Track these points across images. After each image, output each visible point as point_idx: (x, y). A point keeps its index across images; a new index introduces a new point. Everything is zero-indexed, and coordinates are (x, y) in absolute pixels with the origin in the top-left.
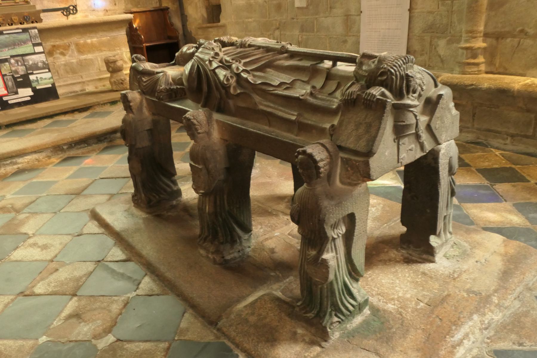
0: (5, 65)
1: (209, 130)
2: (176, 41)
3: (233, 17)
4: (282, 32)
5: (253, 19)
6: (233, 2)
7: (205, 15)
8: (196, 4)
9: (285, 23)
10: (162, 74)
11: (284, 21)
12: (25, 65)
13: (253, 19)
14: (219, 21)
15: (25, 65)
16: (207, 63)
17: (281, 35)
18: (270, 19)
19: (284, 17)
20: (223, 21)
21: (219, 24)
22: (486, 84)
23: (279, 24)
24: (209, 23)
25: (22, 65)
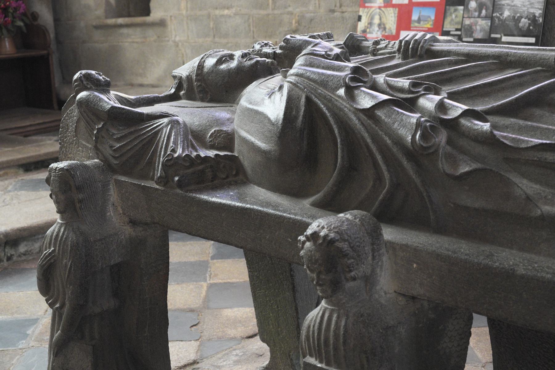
0: (456, 10)
1: (373, 271)
2: (45, 52)
5: (234, 10)
10: (166, 120)
11: (308, 15)
12: (492, 19)
13: (234, 10)
14: (147, 12)
15: (492, 19)
16: (342, 92)
18: (276, 12)
20: (156, 14)
21: (148, 19)
23: (299, 23)
24: (120, 15)
25: (486, 17)
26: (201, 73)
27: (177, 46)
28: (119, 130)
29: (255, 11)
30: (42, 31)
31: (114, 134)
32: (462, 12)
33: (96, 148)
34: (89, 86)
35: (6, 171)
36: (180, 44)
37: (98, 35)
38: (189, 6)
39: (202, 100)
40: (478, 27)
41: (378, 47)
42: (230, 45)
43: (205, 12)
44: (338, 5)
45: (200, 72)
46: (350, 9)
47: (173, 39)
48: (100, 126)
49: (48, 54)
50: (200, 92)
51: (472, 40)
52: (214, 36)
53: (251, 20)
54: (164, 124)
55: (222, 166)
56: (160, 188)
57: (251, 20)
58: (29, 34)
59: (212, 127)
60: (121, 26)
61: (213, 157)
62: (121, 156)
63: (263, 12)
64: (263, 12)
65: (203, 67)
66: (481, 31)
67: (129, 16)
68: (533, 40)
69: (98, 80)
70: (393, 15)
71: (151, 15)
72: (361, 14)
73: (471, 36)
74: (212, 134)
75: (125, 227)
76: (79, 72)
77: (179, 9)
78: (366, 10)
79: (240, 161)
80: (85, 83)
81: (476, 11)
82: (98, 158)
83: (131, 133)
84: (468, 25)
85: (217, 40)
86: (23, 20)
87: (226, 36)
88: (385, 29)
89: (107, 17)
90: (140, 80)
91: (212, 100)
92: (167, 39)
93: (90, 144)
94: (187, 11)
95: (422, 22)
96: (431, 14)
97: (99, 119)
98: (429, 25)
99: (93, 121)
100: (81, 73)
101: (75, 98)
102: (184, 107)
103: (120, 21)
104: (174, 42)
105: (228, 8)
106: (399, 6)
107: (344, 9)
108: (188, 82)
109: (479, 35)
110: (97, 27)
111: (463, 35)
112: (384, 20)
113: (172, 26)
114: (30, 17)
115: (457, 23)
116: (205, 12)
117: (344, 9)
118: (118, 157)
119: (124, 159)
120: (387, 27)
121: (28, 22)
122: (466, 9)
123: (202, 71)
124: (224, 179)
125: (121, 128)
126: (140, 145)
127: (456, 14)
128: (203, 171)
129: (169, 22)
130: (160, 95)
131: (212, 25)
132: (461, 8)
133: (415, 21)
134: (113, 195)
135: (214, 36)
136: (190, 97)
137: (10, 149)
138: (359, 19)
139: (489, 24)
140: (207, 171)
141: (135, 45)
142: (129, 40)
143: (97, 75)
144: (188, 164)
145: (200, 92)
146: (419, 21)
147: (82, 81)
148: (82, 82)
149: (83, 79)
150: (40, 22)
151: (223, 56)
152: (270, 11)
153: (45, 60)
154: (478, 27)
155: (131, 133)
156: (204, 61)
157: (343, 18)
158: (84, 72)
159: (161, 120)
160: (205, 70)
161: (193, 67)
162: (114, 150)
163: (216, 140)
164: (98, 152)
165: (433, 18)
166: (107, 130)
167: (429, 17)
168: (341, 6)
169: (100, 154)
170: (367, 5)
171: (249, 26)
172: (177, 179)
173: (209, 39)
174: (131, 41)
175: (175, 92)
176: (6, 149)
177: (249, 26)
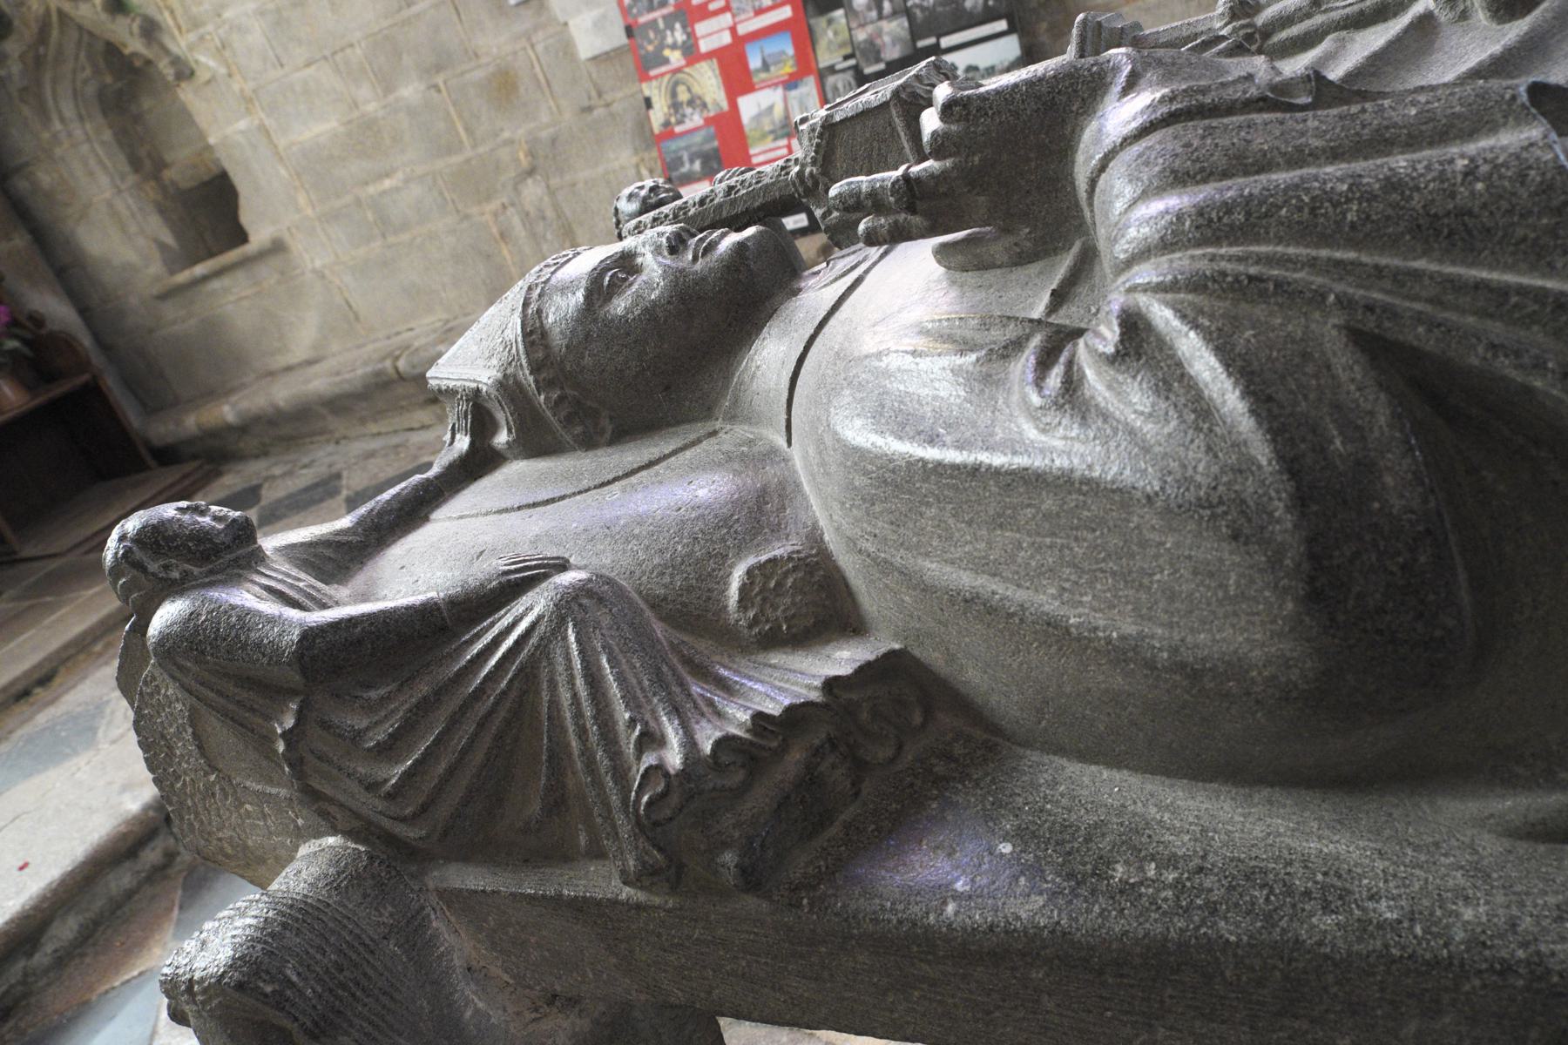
0: (830, 22)
2: (85, 377)
3: (302, 199)
4: (555, 181)
5: (400, 175)
6: (282, 143)
7: (168, 238)
8: (110, 205)
9: (554, 141)
10: (535, 605)
11: (544, 134)
13: (400, 175)
14: (241, 237)
17: (551, 192)
18: (481, 150)
19: (545, 118)
20: (259, 235)
21: (251, 247)
22: (785, 1039)
23: (531, 154)
24: (860, 86)
25: (895, 14)
26: (547, 357)
27: (323, 277)
28: (369, 708)
29: (440, 164)
30: (64, 342)
31: (358, 736)
32: (843, 21)
33: (311, 796)
34: (176, 575)
35: (106, 640)
36: (327, 272)
37: (170, 310)
38: (313, 197)
39: (588, 443)
40: (887, 39)
41: (1260, 20)
42: (419, 240)
43: (348, 199)
44: (594, 93)
45: (540, 355)
46: (619, 95)
47: (310, 266)
48: (289, 722)
49: (94, 377)
50: (568, 421)
51: (882, 66)
52: (384, 236)
53: (440, 182)
54: (542, 628)
55: (864, 716)
56: (657, 900)
57: (440, 182)
58: (40, 355)
59: (722, 561)
60: (205, 279)
61: (815, 696)
62: (424, 808)
63: (456, 159)
64: (456, 159)
65: (544, 334)
66: (894, 44)
67: (211, 255)
68: (1002, 25)
69: (202, 536)
70: (710, 73)
71: (252, 238)
72: (647, 93)
73: (878, 60)
74: (743, 590)
75: (546, 1025)
76: (115, 534)
77: (298, 210)
78: (654, 83)
79: (917, 662)
80: (153, 567)
81: (869, 9)
82: (334, 831)
83: (425, 707)
84: (865, 41)
85: (391, 239)
86: (16, 337)
87: (405, 226)
88: (704, 105)
89: (172, 272)
90: (281, 361)
91: (625, 431)
92: (298, 271)
93: (279, 785)
94: (314, 207)
95: (772, 68)
96: (784, 46)
97: (276, 693)
98: (789, 68)
99: (252, 710)
100: (122, 538)
101: (144, 633)
102: (553, 501)
103: (199, 270)
104: (314, 271)
105: (387, 175)
106: (717, 54)
107: (608, 97)
108: (512, 400)
109: (893, 53)
110: (165, 296)
111: (862, 64)
112: (696, 89)
113: (297, 245)
114: (29, 324)
115: (842, 45)
116: (348, 199)
117: (608, 97)
118: (415, 816)
119: (443, 811)
120: (708, 100)
121: (28, 336)
122: (851, 12)
123: (547, 347)
124: (892, 760)
125: (373, 694)
126: (487, 740)
127: (832, 34)
128: (810, 780)
129: (287, 238)
130: (431, 474)
131: (370, 216)
132: (839, 13)
133: (758, 71)
134: (456, 943)
135: (384, 236)
136: (537, 441)
137: (97, 589)
138: (648, 103)
139: (906, 24)
140: (822, 768)
141: (245, 303)
142: (232, 298)
143: (186, 517)
144: (739, 776)
145: (568, 421)
146: (766, 66)
147: (139, 566)
148: (144, 569)
149: (139, 554)
150: (52, 326)
151: (596, 277)
152: (469, 153)
153: (94, 391)
154: (887, 39)
155: (425, 707)
156: (539, 311)
157: (612, 115)
158: (132, 524)
159: (518, 607)
160: (558, 340)
161: (507, 345)
162: (390, 796)
163: (775, 608)
164: (325, 806)
165: (790, 51)
166: (325, 725)
167: (783, 53)
168: (600, 94)
169: (332, 809)
170: (653, 73)
171: (441, 193)
172: (729, 858)
173: (377, 245)
174: (235, 300)
175: (472, 444)
176: (91, 592)
177: (441, 193)
